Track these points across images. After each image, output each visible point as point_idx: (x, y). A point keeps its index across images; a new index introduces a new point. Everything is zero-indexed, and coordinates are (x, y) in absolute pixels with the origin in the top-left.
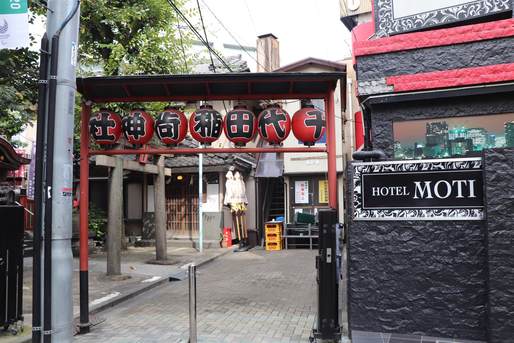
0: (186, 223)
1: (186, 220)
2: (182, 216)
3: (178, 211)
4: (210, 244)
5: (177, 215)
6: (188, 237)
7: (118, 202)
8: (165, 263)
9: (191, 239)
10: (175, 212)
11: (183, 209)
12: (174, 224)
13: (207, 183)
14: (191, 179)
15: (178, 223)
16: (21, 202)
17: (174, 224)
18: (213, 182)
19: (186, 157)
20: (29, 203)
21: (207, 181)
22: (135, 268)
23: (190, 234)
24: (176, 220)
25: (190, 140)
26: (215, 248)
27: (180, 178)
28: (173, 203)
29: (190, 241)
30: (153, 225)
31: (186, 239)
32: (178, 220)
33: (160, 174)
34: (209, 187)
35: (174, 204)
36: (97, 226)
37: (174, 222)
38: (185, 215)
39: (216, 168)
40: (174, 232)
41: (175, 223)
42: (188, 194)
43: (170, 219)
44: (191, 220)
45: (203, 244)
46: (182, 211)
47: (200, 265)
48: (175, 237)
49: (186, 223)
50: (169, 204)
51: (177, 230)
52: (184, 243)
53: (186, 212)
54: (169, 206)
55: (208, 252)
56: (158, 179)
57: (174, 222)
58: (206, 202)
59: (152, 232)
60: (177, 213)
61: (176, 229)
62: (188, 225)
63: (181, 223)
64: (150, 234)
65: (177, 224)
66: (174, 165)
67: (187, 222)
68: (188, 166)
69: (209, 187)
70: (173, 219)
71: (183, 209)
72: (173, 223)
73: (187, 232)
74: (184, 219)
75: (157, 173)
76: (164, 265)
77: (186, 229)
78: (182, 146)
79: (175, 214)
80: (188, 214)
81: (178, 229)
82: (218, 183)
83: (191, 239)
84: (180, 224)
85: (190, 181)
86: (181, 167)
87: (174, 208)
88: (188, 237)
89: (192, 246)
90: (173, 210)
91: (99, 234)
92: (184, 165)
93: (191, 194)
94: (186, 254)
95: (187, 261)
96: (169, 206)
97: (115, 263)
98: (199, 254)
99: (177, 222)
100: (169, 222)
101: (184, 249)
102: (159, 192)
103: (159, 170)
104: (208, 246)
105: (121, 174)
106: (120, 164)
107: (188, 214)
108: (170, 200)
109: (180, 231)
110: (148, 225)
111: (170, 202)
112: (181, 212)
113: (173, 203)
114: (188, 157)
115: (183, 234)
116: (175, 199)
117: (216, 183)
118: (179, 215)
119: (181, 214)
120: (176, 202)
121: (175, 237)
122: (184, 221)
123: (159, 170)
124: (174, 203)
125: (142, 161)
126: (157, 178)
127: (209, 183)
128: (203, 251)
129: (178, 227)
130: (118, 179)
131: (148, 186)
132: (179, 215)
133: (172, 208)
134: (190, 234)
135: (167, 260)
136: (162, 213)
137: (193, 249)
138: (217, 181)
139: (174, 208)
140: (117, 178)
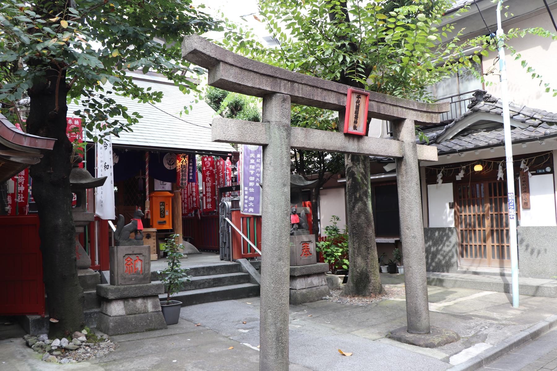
0: (493, 246)
1: (493, 241)
2: (487, 233)
3: (479, 226)
4: (538, 288)
5: (477, 232)
6: (497, 270)
7: (276, 222)
8: (422, 343)
9: (502, 275)
10: (474, 226)
11: (487, 222)
12: (473, 247)
13: (529, 174)
14: (498, 169)
15: (480, 246)
16: (233, 218)
17: (473, 247)
18: (540, 171)
19: (487, 131)
20: (245, 219)
21: (530, 170)
22: (348, 354)
23: (502, 266)
24: (475, 241)
25: (493, 102)
26: (550, 297)
27: (478, 168)
28: (470, 211)
29: (499, 279)
30: (437, 250)
31: (495, 274)
32: (480, 240)
33: (406, 158)
34: (534, 180)
35: (472, 214)
36: (341, 253)
37: (473, 243)
38: (492, 231)
39: (544, 143)
40: (473, 262)
41: (475, 246)
42: (495, 195)
43: (466, 239)
44: (502, 241)
45: (521, 287)
46: (486, 226)
47: (501, 351)
48: (474, 270)
49: (493, 246)
50: (463, 214)
51: (478, 258)
52: (489, 284)
53: (492, 226)
54: (463, 217)
55: (531, 310)
56: (403, 167)
57: (473, 243)
58: (529, 208)
59: (436, 260)
60: (477, 228)
61: (476, 256)
62: (498, 250)
63: (485, 246)
64: (434, 264)
65: (478, 246)
66: (464, 147)
67: (496, 244)
68: (489, 146)
69: (534, 180)
70: (471, 239)
71: (487, 222)
72: (471, 246)
73: (496, 261)
74: (490, 239)
75: (398, 155)
76: (419, 346)
77: (494, 257)
78: (478, 114)
79: (475, 231)
80: (497, 231)
81: (481, 256)
82: (552, 172)
83: (502, 275)
84: (482, 247)
85: (497, 173)
86: (477, 148)
87: (472, 220)
88: (497, 270)
89: (503, 290)
90: (470, 225)
91: (345, 264)
92: (482, 144)
93: (495, 195)
94: (482, 313)
95: (476, 335)
96: (463, 217)
97: (272, 358)
98: (511, 313)
99: (478, 244)
100: (464, 244)
101: (485, 297)
102: (406, 194)
103: (402, 148)
104: (534, 290)
105: (281, 159)
106: (277, 136)
107: (497, 231)
108: (465, 207)
109: (484, 259)
110: (431, 249)
111: (465, 211)
112: (484, 226)
113: (470, 211)
114: (491, 130)
115: (489, 264)
116: (474, 205)
117: (546, 173)
118: (482, 232)
119: (484, 230)
120: (474, 211)
121: (473, 269)
122: (489, 243)
123: (402, 148)
124: (471, 211)
125: (351, 130)
126: (401, 166)
127: (533, 174)
128: (520, 304)
129: (481, 252)
130: (275, 169)
131: (428, 185)
132: (482, 232)
133: (468, 221)
134: (502, 266)
135: (429, 333)
136: (414, 237)
137: (504, 295)
138: (548, 169)
139: (472, 220)
140: (271, 169)
